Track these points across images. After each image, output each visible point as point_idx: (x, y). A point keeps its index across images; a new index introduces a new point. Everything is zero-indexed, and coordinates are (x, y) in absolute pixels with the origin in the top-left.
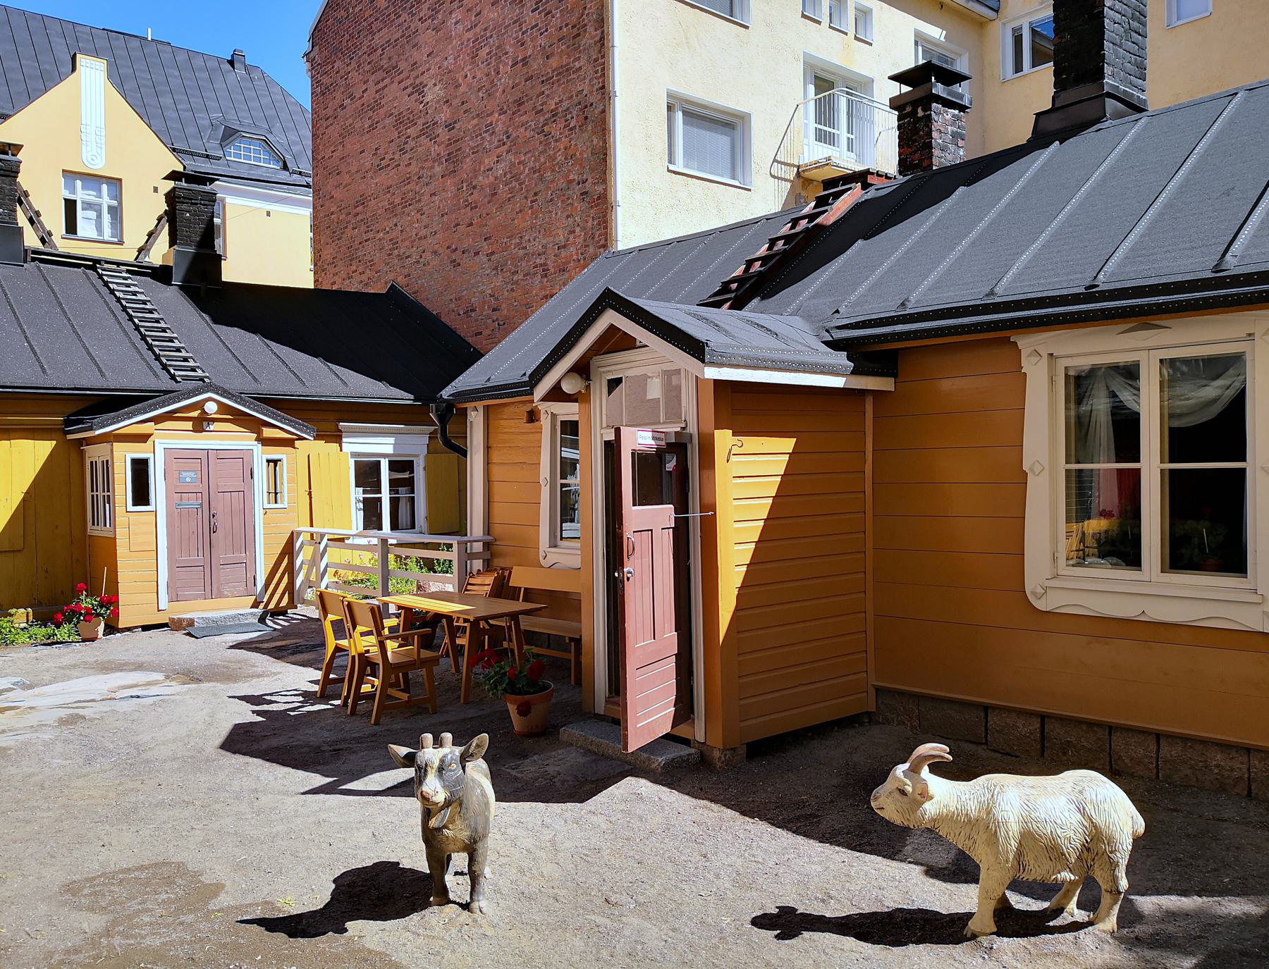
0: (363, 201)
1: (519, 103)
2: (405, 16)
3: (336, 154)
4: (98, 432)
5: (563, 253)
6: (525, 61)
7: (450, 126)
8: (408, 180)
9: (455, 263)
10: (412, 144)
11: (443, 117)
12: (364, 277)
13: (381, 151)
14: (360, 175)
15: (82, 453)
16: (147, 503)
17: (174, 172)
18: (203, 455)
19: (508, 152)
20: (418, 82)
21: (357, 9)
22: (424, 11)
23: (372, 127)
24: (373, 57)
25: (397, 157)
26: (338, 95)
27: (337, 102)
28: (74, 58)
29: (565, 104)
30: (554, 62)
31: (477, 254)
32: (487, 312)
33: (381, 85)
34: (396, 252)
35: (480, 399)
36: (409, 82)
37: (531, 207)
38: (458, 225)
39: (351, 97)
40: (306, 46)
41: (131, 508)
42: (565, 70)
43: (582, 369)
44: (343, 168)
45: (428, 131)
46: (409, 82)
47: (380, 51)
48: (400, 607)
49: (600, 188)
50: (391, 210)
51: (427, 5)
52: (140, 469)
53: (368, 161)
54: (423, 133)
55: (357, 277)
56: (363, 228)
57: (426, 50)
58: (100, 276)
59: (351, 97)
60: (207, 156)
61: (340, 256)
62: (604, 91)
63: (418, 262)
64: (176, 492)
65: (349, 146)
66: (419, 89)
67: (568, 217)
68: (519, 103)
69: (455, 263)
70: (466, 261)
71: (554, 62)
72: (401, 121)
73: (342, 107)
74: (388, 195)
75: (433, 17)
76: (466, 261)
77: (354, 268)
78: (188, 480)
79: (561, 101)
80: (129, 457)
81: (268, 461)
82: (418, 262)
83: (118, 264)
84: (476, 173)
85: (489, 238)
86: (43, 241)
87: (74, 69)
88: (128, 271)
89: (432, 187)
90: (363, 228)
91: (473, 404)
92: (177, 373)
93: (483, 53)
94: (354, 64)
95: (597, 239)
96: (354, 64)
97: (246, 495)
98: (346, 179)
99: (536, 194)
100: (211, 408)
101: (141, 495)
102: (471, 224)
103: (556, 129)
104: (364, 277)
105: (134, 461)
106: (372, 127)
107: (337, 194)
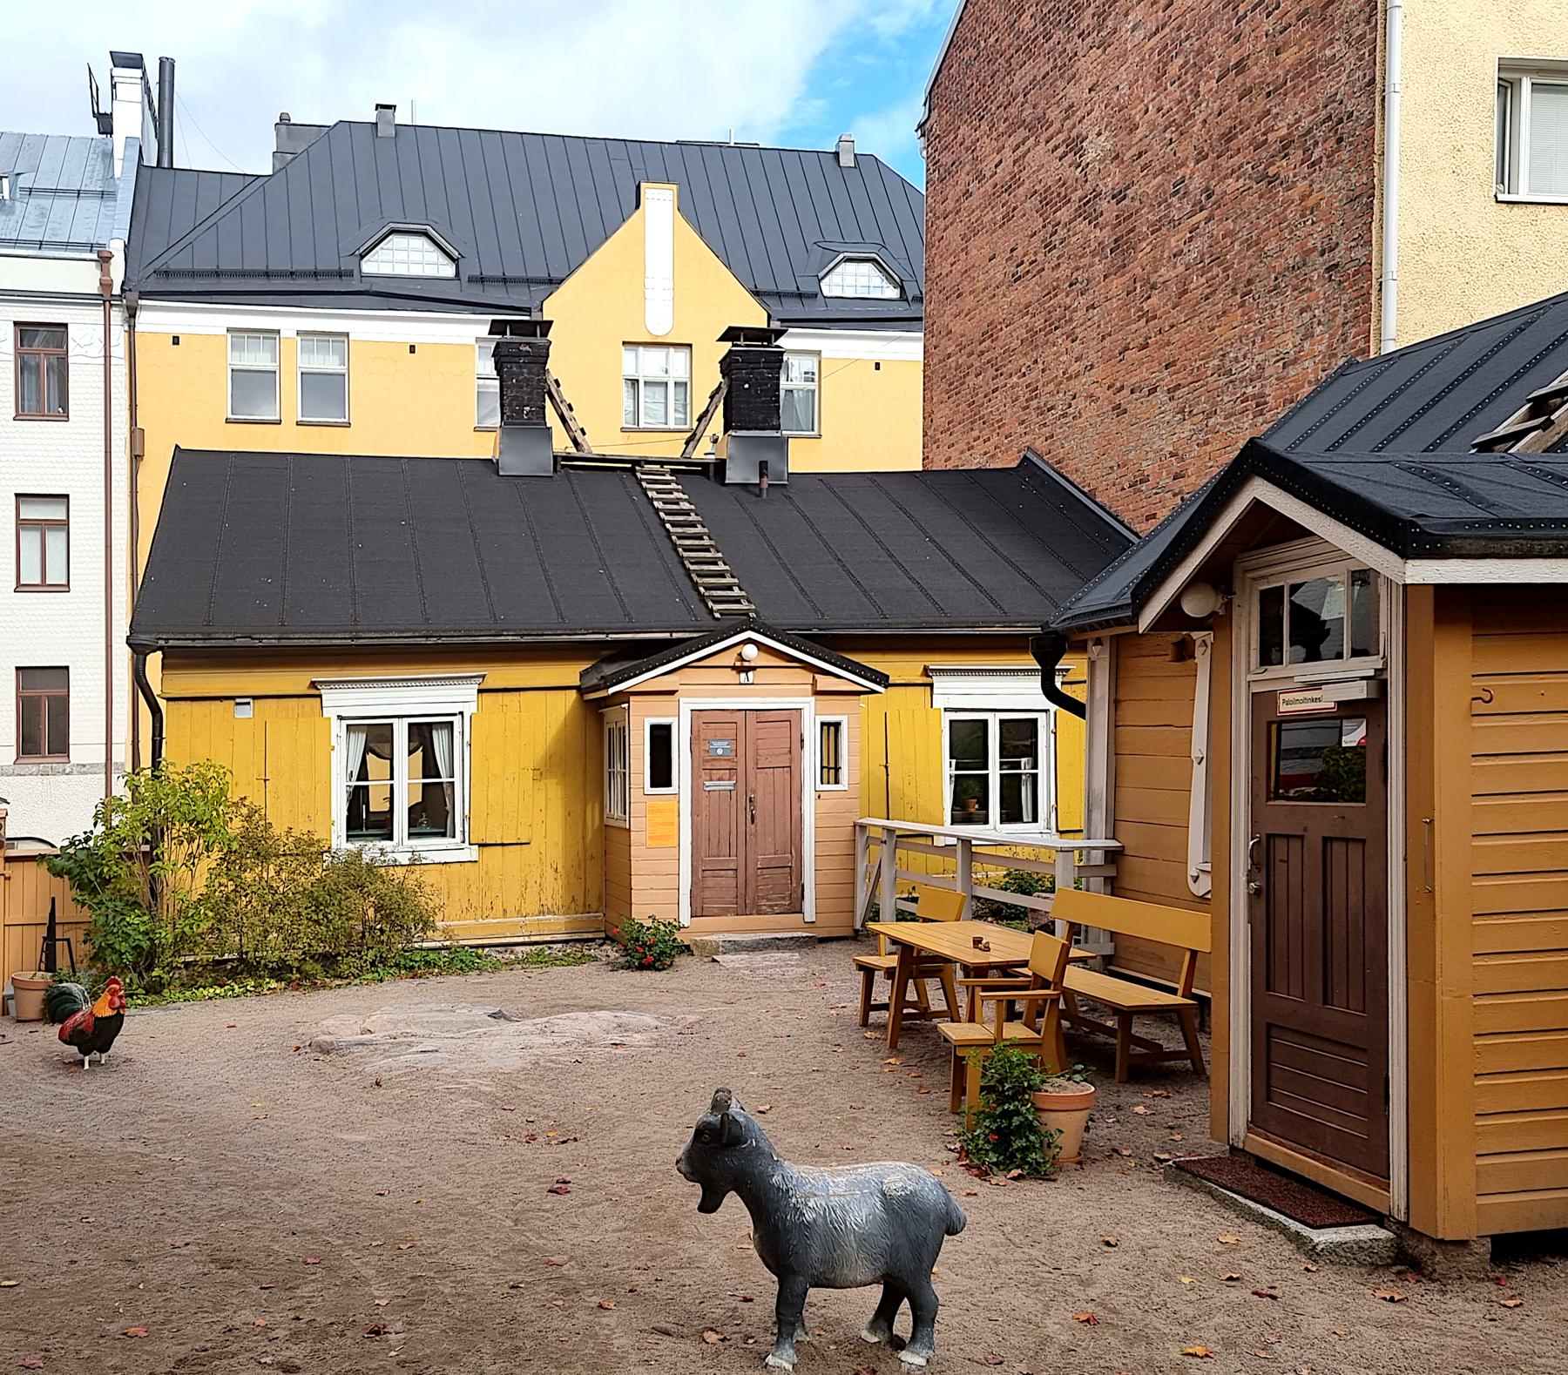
0: (989, 334)
1: (1228, 137)
2: (1058, 35)
3: (958, 267)
4: (612, 690)
5: (1292, 371)
6: (1240, 67)
7: (1119, 196)
8: (1052, 292)
9: (1120, 410)
10: (1062, 233)
11: (1110, 184)
12: (990, 446)
13: (1019, 252)
14: (985, 296)
15: (600, 719)
16: (669, 785)
17: (730, 329)
18: (740, 717)
19: (1208, 220)
20: (1074, 134)
21: (992, 40)
22: (1087, 20)
23: (1007, 218)
24: (1011, 109)
25: (1040, 257)
26: (963, 177)
27: (960, 189)
28: (638, 187)
29: (1305, 123)
30: (1289, 57)
31: (1153, 391)
32: (1166, 480)
33: (1023, 149)
34: (1034, 403)
35: (1107, 624)
36: (1061, 137)
37: (1242, 305)
38: (1126, 349)
39: (980, 178)
40: (920, 113)
41: (649, 790)
42: (1307, 69)
43: (1216, 575)
44: (966, 287)
45: (1087, 210)
46: (1061, 137)
47: (1020, 99)
48: (894, 941)
49: (1358, 253)
50: (1031, 339)
51: (1091, 10)
52: (661, 737)
53: (999, 270)
54: (1079, 213)
55: (980, 447)
56: (991, 372)
57: (1087, 82)
58: (639, 481)
59: (980, 178)
60: (800, 296)
61: (959, 417)
62: (1373, 87)
63: (1064, 415)
64: (704, 766)
65: (974, 252)
66: (1075, 145)
67: (1302, 311)
68: (1228, 137)
69: (1120, 410)
70: (1137, 406)
71: (1289, 57)
72: (1048, 201)
73: (967, 194)
74: (1026, 319)
75: (1100, 27)
76: (1137, 406)
77: (975, 433)
78: (720, 752)
79: (1298, 121)
80: (649, 721)
81: (823, 724)
82: (1064, 415)
83: (662, 463)
84: (1156, 263)
85: (1173, 364)
86: (576, 443)
87: (638, 206)
88: (673, 472)
89: (1089, 297)
90: (991, 372)
91: (1096, 634)
92: (716, 607)
93: (1173, 69)
94: (984, 126)
95: (1350, 340)
96: (984, 126)
97: (792, 770)
98: (970, 301)
99: (1250, 282)
100: (750, 651)
101: (661, 774)
102: (1146, 346)
103: (1282, 167)
104: (990, 446)
105: (653, 728)
106: (1007, 218)
107: (957, 327)
